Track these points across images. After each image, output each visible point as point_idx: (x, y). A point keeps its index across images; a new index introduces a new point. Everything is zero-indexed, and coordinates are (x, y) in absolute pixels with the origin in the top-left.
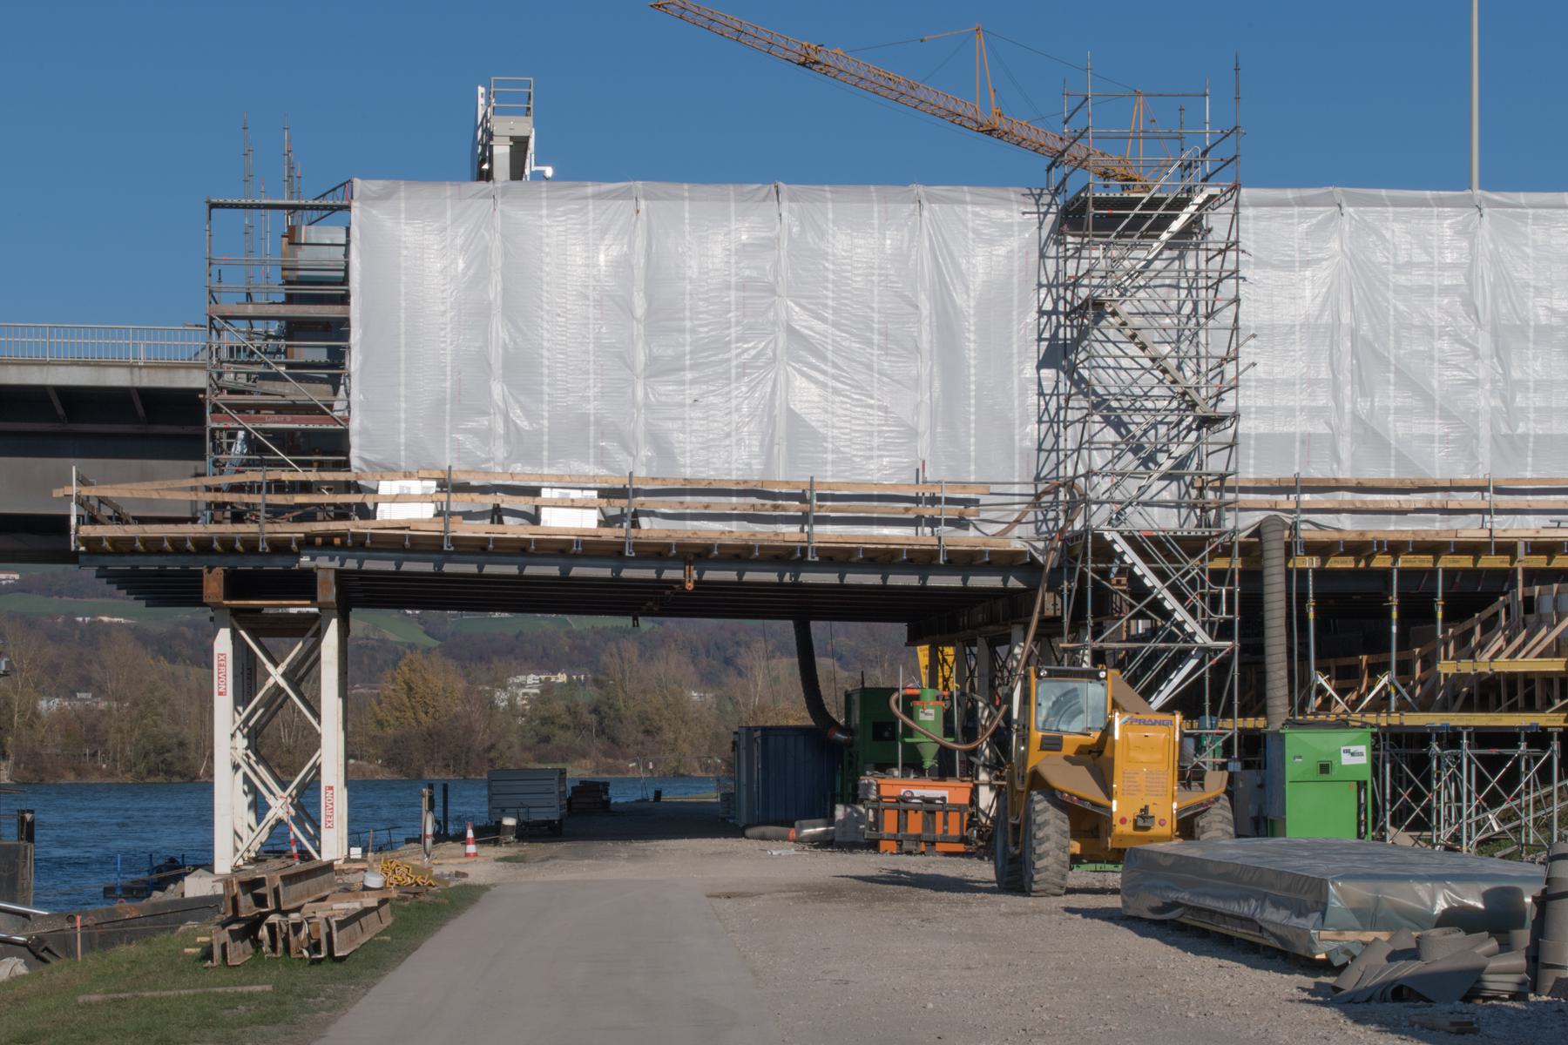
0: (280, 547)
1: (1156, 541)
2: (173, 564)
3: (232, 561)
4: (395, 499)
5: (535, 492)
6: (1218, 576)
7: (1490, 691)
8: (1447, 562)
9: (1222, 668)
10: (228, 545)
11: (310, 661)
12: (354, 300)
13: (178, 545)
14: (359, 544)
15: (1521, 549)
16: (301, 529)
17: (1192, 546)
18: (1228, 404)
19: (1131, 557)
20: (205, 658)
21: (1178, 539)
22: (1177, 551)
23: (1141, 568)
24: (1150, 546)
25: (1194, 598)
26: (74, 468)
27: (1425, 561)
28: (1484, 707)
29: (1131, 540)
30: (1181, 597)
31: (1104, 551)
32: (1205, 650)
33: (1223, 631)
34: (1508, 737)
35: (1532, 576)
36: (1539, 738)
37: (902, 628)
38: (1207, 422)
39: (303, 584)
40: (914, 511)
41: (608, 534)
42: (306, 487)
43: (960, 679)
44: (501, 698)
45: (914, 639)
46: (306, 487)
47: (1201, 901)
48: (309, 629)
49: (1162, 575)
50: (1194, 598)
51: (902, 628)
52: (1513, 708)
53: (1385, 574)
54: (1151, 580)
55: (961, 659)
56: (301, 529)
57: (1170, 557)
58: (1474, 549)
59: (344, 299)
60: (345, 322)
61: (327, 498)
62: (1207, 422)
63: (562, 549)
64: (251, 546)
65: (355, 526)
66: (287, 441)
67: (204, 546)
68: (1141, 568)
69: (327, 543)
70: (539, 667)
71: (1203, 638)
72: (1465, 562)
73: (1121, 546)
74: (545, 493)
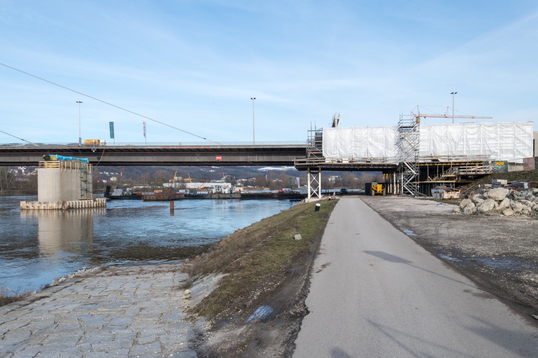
0: (315, 165)
1: (410, 163)
2: (305, 167)
3: (310, 167)
4: (327, 160)
5: (325, 159)
6: (417, 166)
7: (448, 179)
8: (443, 164)
9: (417, 177)
10: (310, 165)
11: (318, 176)
12: (323, 140)
13: (305, 165)
14: (323, 165)
15: (452, 163)
16: (317, 164)
17: (414, 163)
18: (418, 148)
19: (407, 165)
20: (307, 177)
21: (412, 163)
22: (412, 164)
23: (408, 166)
24: (409, 164)
25: (414, 169)
26: (121, 175)
27: (441, 164)
28: (448, 180)
29: (407, 163)
30: (413, 169)
31: (404, 164)
32: (416, 175)
33: (417, 172)
34: (449, 183)
35: (453, 166)
36: (453, 183)
37: (382, 172)
38: (415, 150)
39: (317, 169)
40: (423, 159)
41: (350, 163)
42: (317, 159)
43: (388, 177)
44: (330, 179)
45: (383, 173)
46: (317, 159)
47: (218, 168)
48: (317, 173)
49: (410, 166)
50: (414, 169)
51: (382, 172)
52: (450, 180)
53: (437, 166)
54: (409, 167)
55: (388, 175)
56: (317, 164)
57: (411, 164)
58: (447, 163)
59: (322, 140)
60: (322, 142)
61: (320, 160)
62: (415, 150)
63: (345, 165)
64: (312, 165)
65: (323, 163)
66: (316, 155)
67: (308, 165)
68: (408, 166)
69: (320, 165)
70: (334, 175)
71: (415, 173)
72: (445, 164)
73: (406, 164)
74: (326, 159)
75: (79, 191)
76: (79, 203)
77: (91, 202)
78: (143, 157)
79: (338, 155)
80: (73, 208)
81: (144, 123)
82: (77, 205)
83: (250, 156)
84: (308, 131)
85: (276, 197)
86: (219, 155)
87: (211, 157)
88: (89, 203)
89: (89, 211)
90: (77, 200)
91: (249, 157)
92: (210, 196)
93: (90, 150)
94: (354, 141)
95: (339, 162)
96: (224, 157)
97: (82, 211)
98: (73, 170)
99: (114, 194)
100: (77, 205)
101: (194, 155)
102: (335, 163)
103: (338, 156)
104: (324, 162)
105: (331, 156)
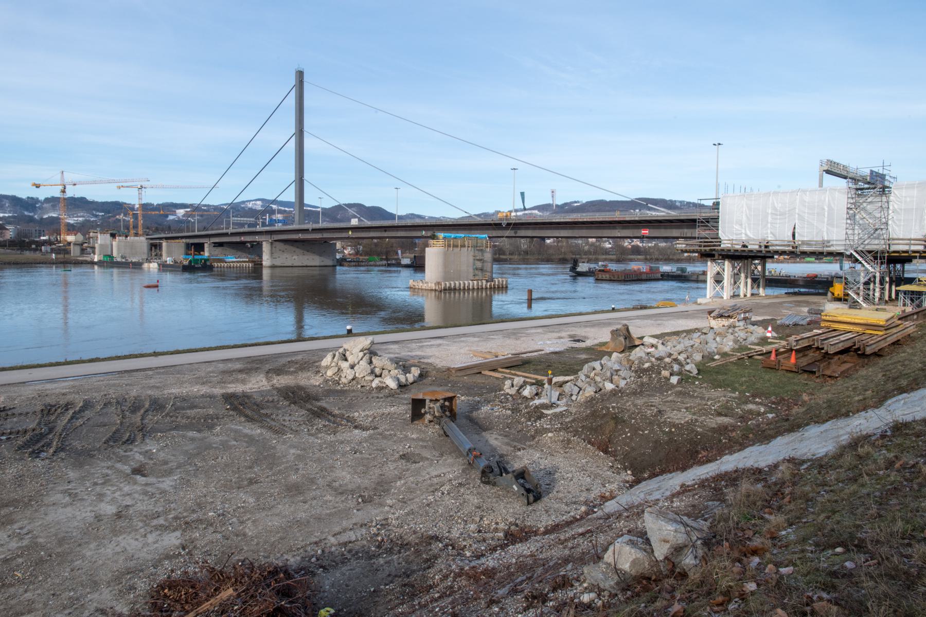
63: (751, 251)
75: (471, 270)
76: (469, 284)
77: (482, 283)
78: (558, 231)
79: (743, 235)
80: (455, 289)
81: (553, 192)
82: (462, 286)
83: (687, 228)
84: (157, 286)
85: (801, 283)
86: (645, 228)
87: (636, 231)
88: (480, 284)
89: (480, 293)
90: (467, 280)
91: (686, 230)
92: (696, 277)
93: (500, 224)
94: (772, 213)
95: (744, 246)
96: (652, 230)
97: (473, 293)
98: (462, 249)
99: (579, 269)
100: (462, 286)
101: (614, 228)
102: (738, 247)
103: (744, 238)
104: (720, 245)
105: (731, 238)
